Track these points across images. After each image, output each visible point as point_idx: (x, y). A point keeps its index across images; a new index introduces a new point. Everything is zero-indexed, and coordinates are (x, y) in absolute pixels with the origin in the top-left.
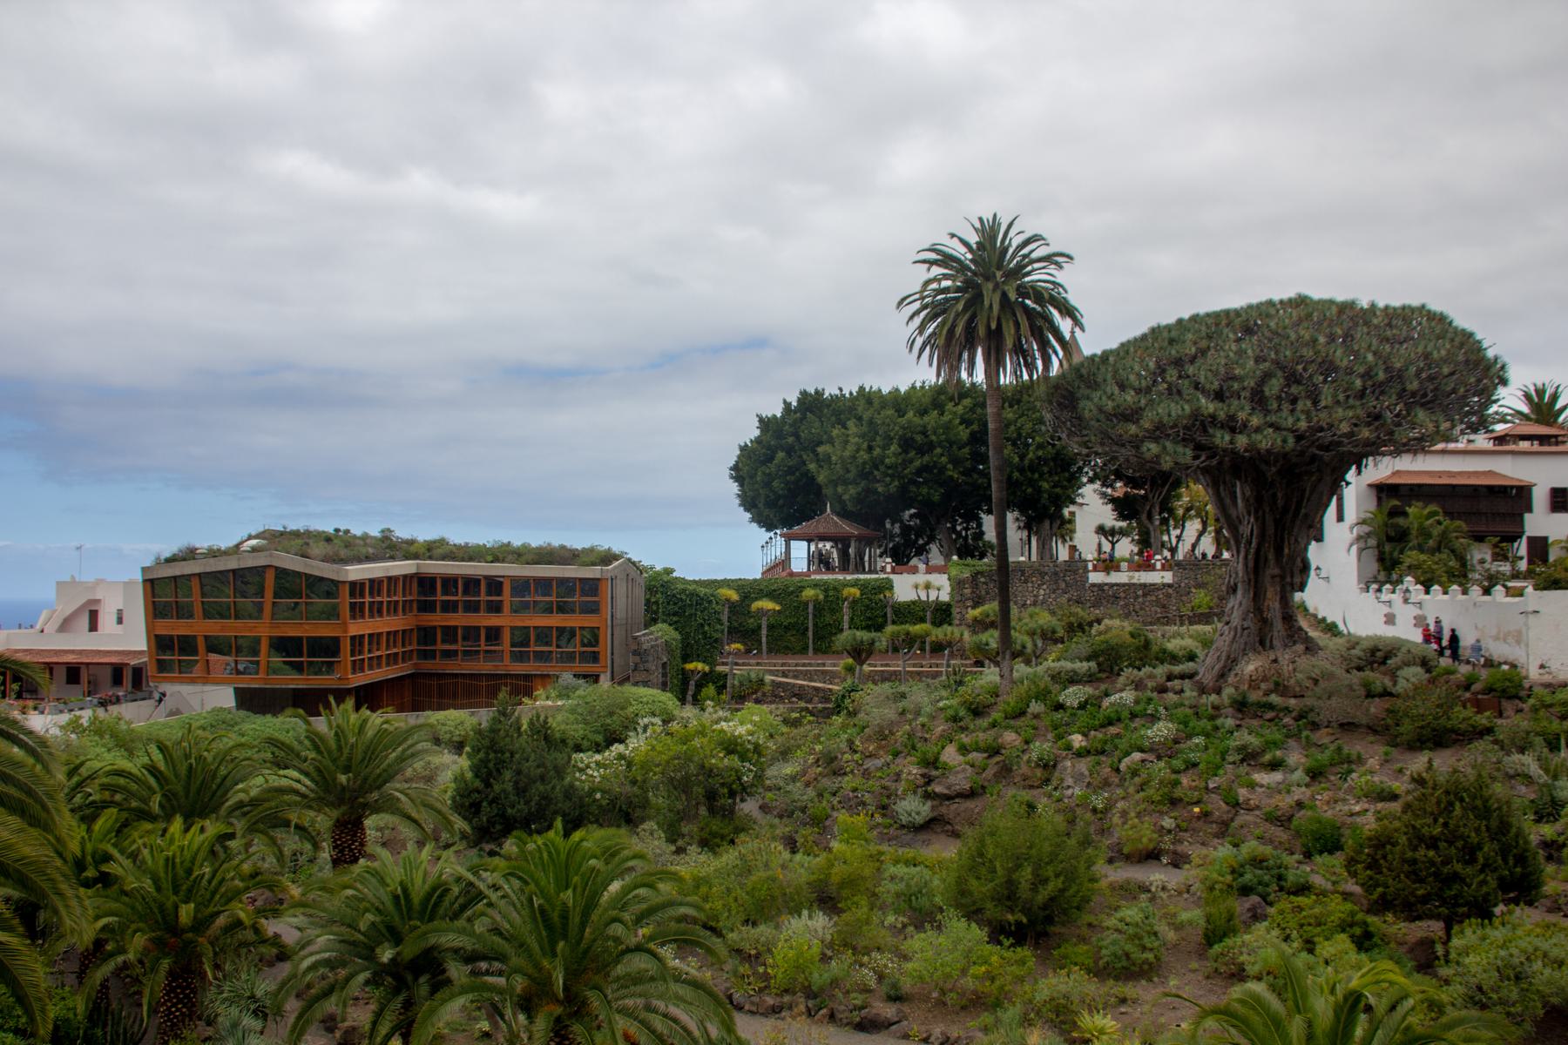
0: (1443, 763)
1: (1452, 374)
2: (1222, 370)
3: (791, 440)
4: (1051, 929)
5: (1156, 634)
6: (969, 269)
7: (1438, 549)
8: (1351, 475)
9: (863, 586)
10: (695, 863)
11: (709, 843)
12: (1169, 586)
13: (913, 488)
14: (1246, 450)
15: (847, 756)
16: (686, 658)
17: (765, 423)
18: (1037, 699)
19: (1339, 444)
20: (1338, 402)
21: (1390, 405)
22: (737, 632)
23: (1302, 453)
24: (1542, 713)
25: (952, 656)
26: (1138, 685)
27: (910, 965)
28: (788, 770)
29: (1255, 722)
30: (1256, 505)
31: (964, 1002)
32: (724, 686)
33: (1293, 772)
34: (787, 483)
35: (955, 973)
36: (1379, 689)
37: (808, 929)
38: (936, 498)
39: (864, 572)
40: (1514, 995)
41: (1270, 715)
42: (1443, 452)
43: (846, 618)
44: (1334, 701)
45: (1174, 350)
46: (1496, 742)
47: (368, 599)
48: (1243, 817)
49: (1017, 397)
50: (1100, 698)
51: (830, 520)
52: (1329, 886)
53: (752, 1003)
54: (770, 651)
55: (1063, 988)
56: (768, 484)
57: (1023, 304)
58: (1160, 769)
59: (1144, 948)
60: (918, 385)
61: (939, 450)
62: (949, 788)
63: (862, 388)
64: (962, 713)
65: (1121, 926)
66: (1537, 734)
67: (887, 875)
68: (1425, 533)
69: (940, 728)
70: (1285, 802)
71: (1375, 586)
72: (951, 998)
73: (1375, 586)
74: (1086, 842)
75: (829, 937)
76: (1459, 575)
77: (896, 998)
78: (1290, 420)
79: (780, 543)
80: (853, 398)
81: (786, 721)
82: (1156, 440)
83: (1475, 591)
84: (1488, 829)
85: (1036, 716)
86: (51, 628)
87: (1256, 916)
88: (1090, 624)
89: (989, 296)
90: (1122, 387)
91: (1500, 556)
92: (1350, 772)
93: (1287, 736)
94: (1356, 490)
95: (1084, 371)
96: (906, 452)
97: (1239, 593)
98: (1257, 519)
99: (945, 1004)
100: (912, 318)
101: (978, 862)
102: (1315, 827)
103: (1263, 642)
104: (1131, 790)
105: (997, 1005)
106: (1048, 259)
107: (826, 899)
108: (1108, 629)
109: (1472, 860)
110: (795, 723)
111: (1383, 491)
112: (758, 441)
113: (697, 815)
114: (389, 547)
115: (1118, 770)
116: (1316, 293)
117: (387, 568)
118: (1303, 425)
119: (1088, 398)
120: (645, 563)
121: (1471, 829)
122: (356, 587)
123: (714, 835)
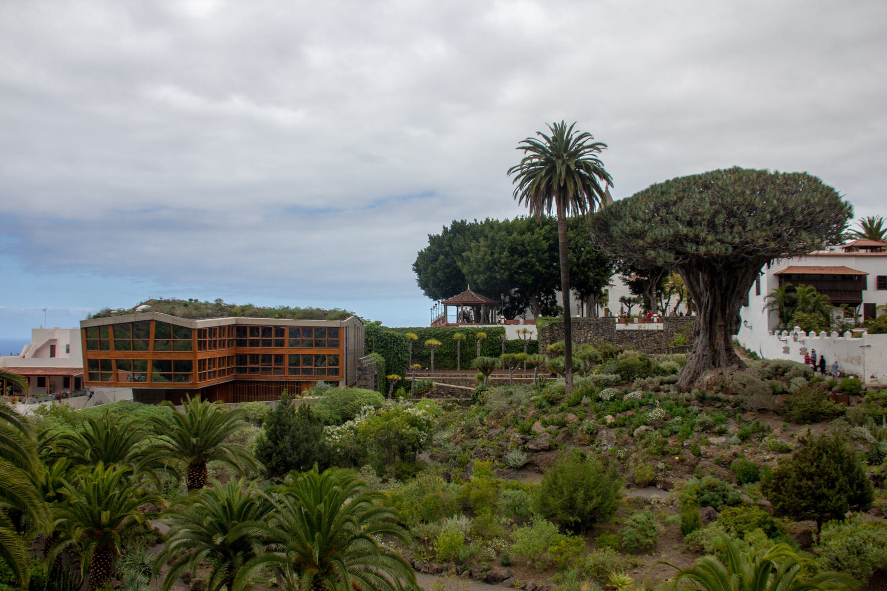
0: (817, 432)
1: (822, 211)
2: (691, 209)
3: (447, 249)
4: (595, 525)
5: (654, 358)
6: (548, 152)
7: (814, 311)
8: (764, 269)
9: (488, 331)
10: (393, 488)
11: (401, 477)
12: (662, 331)
13: (516, 276)
14: (705, 255)
15: (479, 428)
16: (388, 372)
17: (433, 239)
18: (587, 395)
19: (758, 251)
20: (757, 227)
21: (786, 229)
22: (417, 358)
23: (736, 256)
24: (872, 403)
25: (538, 371)
26: (644, 388)
27: (515, 546)
28: (446, 435)
29: (710, 409)
30: (711, 285)
31: (545, 567)
32: (410, 388)
33: (731, 436)
34: (445, 273)
35: (540, 550)
36: (780, 390)
37: (457, 525)
38: (530, 282)
39: (489, 323)
40: (857, 563)
41: (718, 404)
42: (817, 256)
43: (479, 349)
44: (754, 396)
45: (664, 198)
46: (846, 420)
47: (208, 339)
48: (703, 462)
49: (575, 225)
50: (622, 395)
51: (469, 294)
52: (752, 501)
53: (426, 567)
54: (435, 368)
55: (601, 559)
56: (434, 274)
57: (579, 172)
58: (656, 435)
59: (647, 536)
60: (519, 218)
61: (531, 255)
62: (537, 446)
63: (487, 220)
64: (544, 403)
65: (634, 523)
66: (870, 415)
67: (502, 495)
68: (806, 302)
69: (532, 412)
70: (727, 454)
71: (778, 332)
72: (538, 564)
73: (778, 332)
74: (614, 476)
75: (469, 530)
76: (826, 325)
77: (507, 564)
78: (730, 238)
79: (441, 307)
80: (482, 225)
81: (444, 408)
82: (654, 249)
83: (835, 334)
84: (842, 469)
85: (586, 405)
86: (29, 355)
87: (710, 518)
88: (617, 353)
89: (560, 167)
90: (635, 219)
91: (849, 314)
92: (764, 436)
93: (728, 416)
94: (767, 277)
95: (613, 210)
96: (512, 255)
97: (701, 335)
98: (711, 294)
99: (534, 568)
100: (516, 180)
101: (553, 487)
102: (744, 467)
103: (714, 363)
104: (640, 447)
105: (564, 568)
106: (593, 146)
107: (468, 509)
108: (627, 356)
109: (833, 487)
110: (450, 409)
111: (782, 277)
112: (429, 249)
113: (394, 461)
114: (220, 309)
115: (632, 436)
116: (745, 166)
117: (219, 321)
118: (737, 240)
119: (615, 225)
120: (365, 318)
121: (832, 469)
122: (202, 332)
123: (404, 472)
